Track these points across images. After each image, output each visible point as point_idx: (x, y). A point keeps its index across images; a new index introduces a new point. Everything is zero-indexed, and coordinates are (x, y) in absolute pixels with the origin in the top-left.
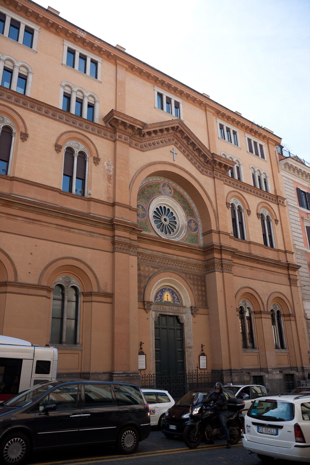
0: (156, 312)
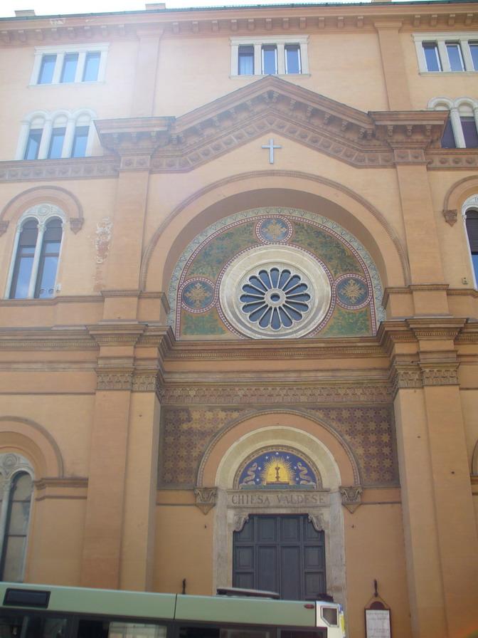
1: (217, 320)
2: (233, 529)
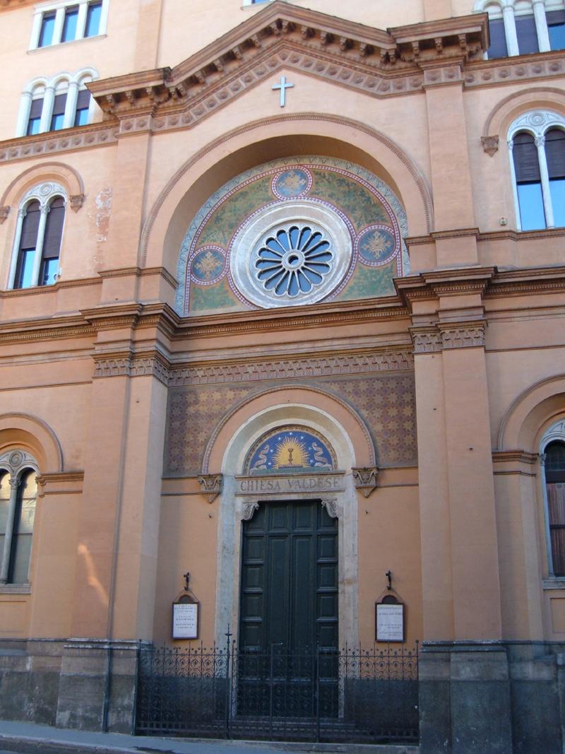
0: (246, 497)
1: (227, 291)
2: (242, 518)
